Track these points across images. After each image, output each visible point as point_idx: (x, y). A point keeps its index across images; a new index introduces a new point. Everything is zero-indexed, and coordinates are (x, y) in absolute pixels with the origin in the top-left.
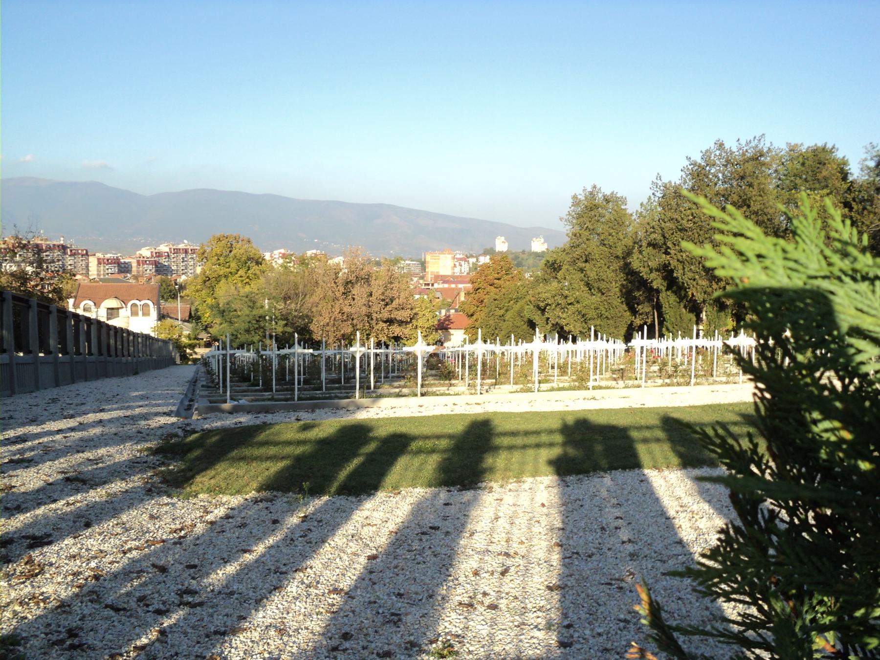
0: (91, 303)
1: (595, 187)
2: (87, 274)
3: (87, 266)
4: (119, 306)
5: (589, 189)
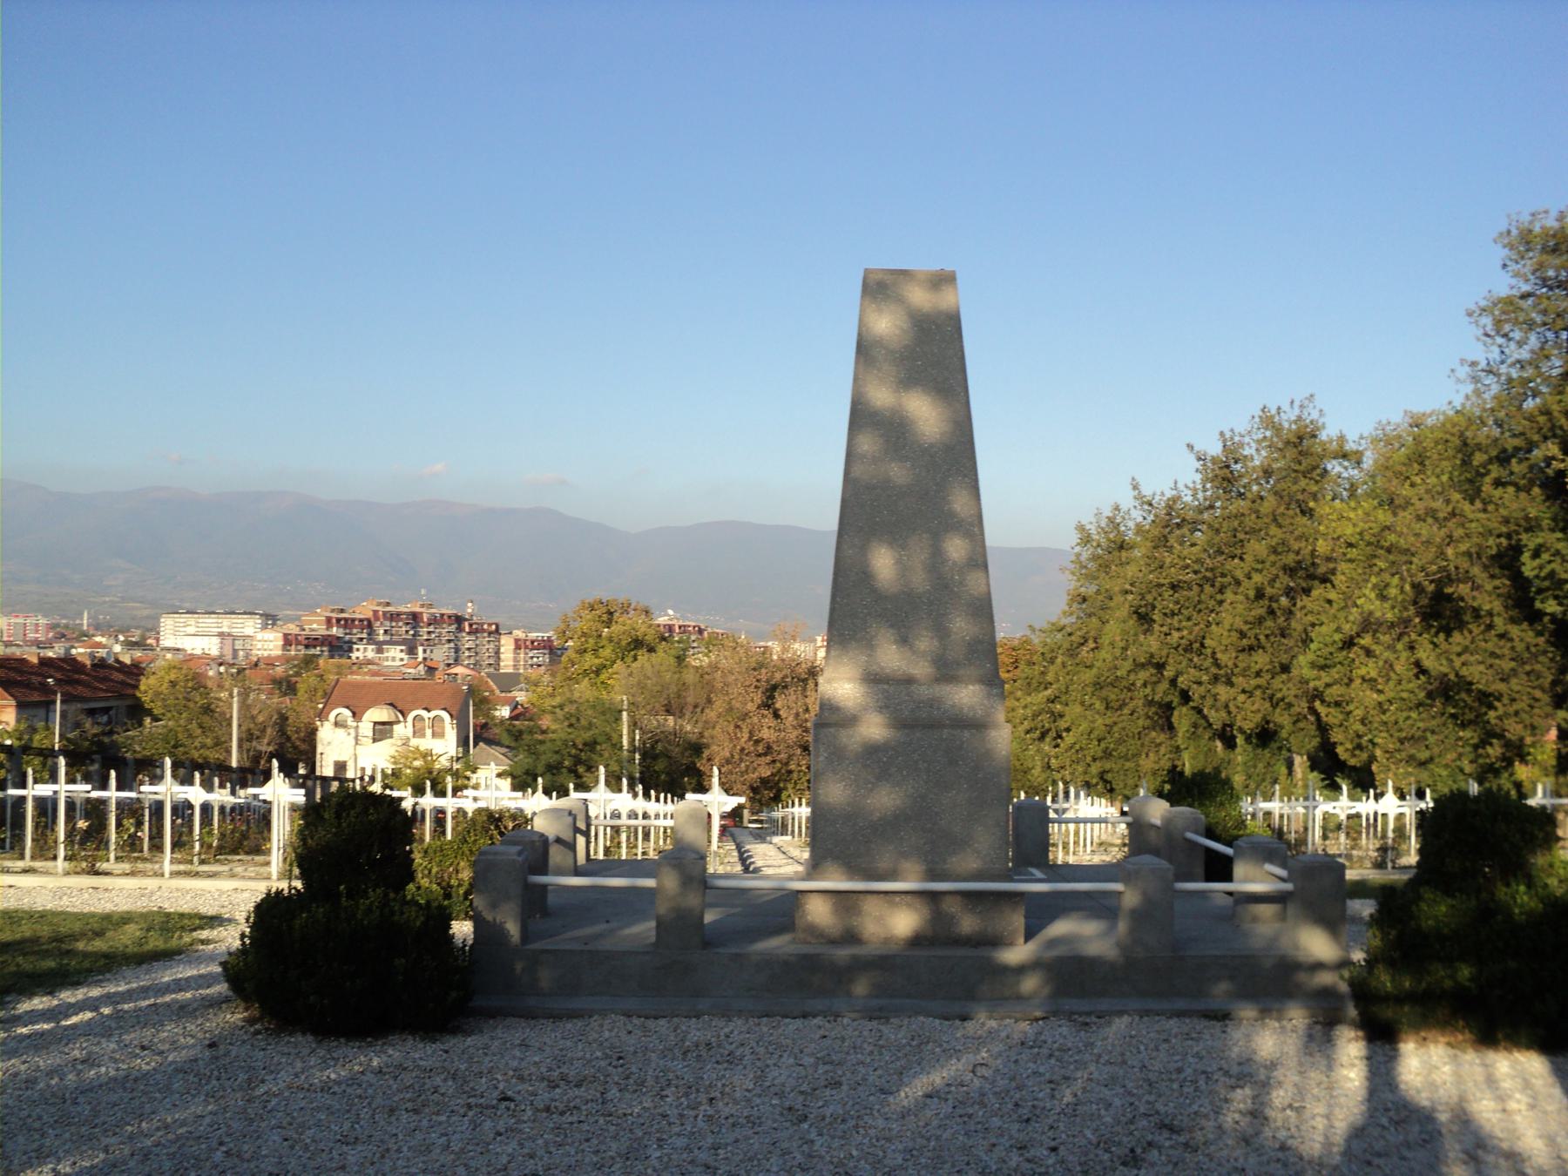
0: (347, 713)
1: (1117, 508)
2: (497, 665)
3: (497, 652)
4: (393, 719)
5: (1108, 512)
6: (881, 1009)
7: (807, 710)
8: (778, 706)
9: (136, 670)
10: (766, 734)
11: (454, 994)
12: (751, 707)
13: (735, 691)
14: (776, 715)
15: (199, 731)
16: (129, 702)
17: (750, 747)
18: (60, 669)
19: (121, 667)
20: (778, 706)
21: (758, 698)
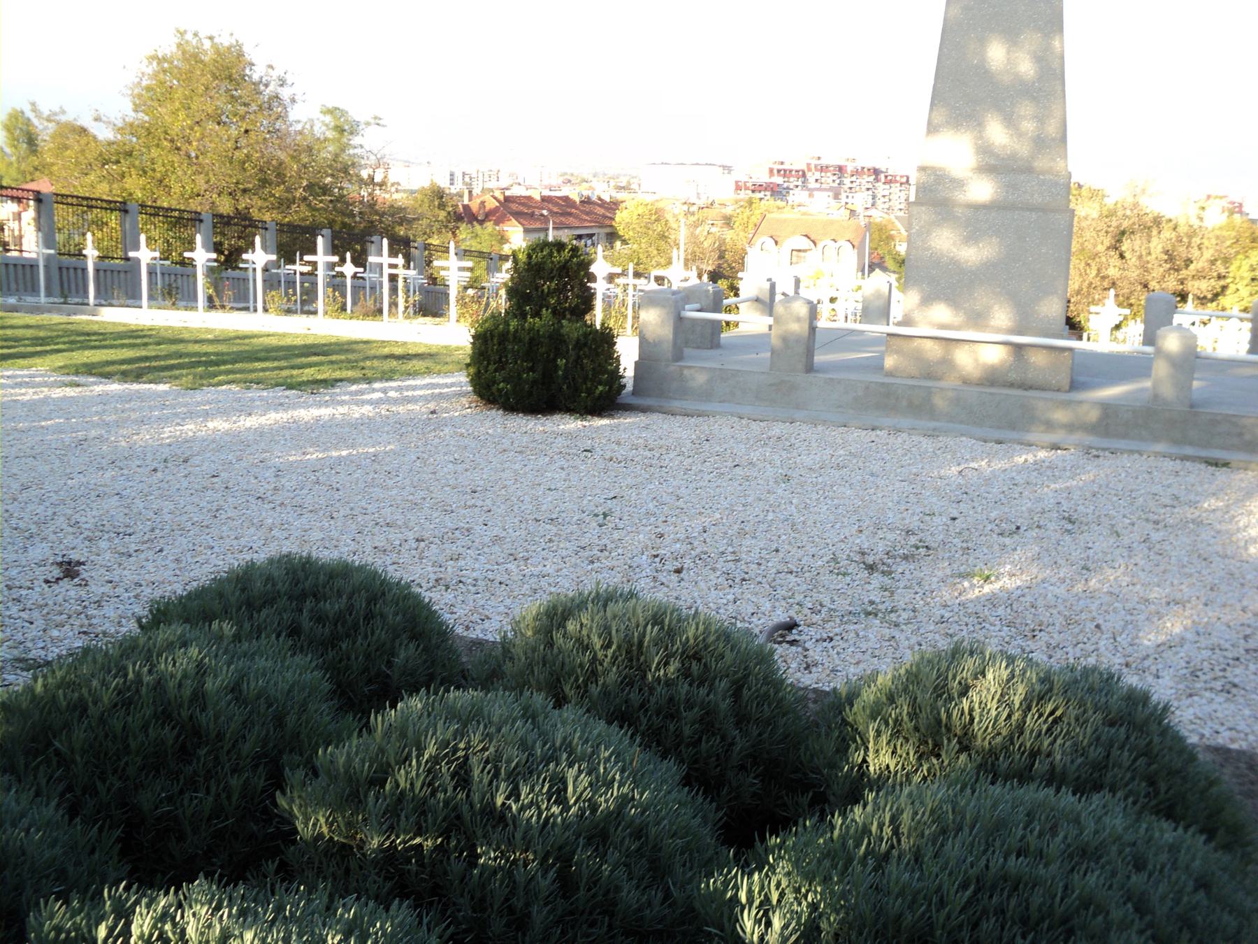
6: (934, 430)
7: (1149, 254)
8: (1123, 248)
9: (614, 206)
10: (1113, 272)
11: (601, 388)
12: (1100, 248)
13: (1088, 234)
14: (1122, 256)
15: (655, 252)
16: (608, 230)
17: (1097, 282)
18: (557, 204)
19: (602, 204)
20: (1123, 248)
21: (1108, 241)
